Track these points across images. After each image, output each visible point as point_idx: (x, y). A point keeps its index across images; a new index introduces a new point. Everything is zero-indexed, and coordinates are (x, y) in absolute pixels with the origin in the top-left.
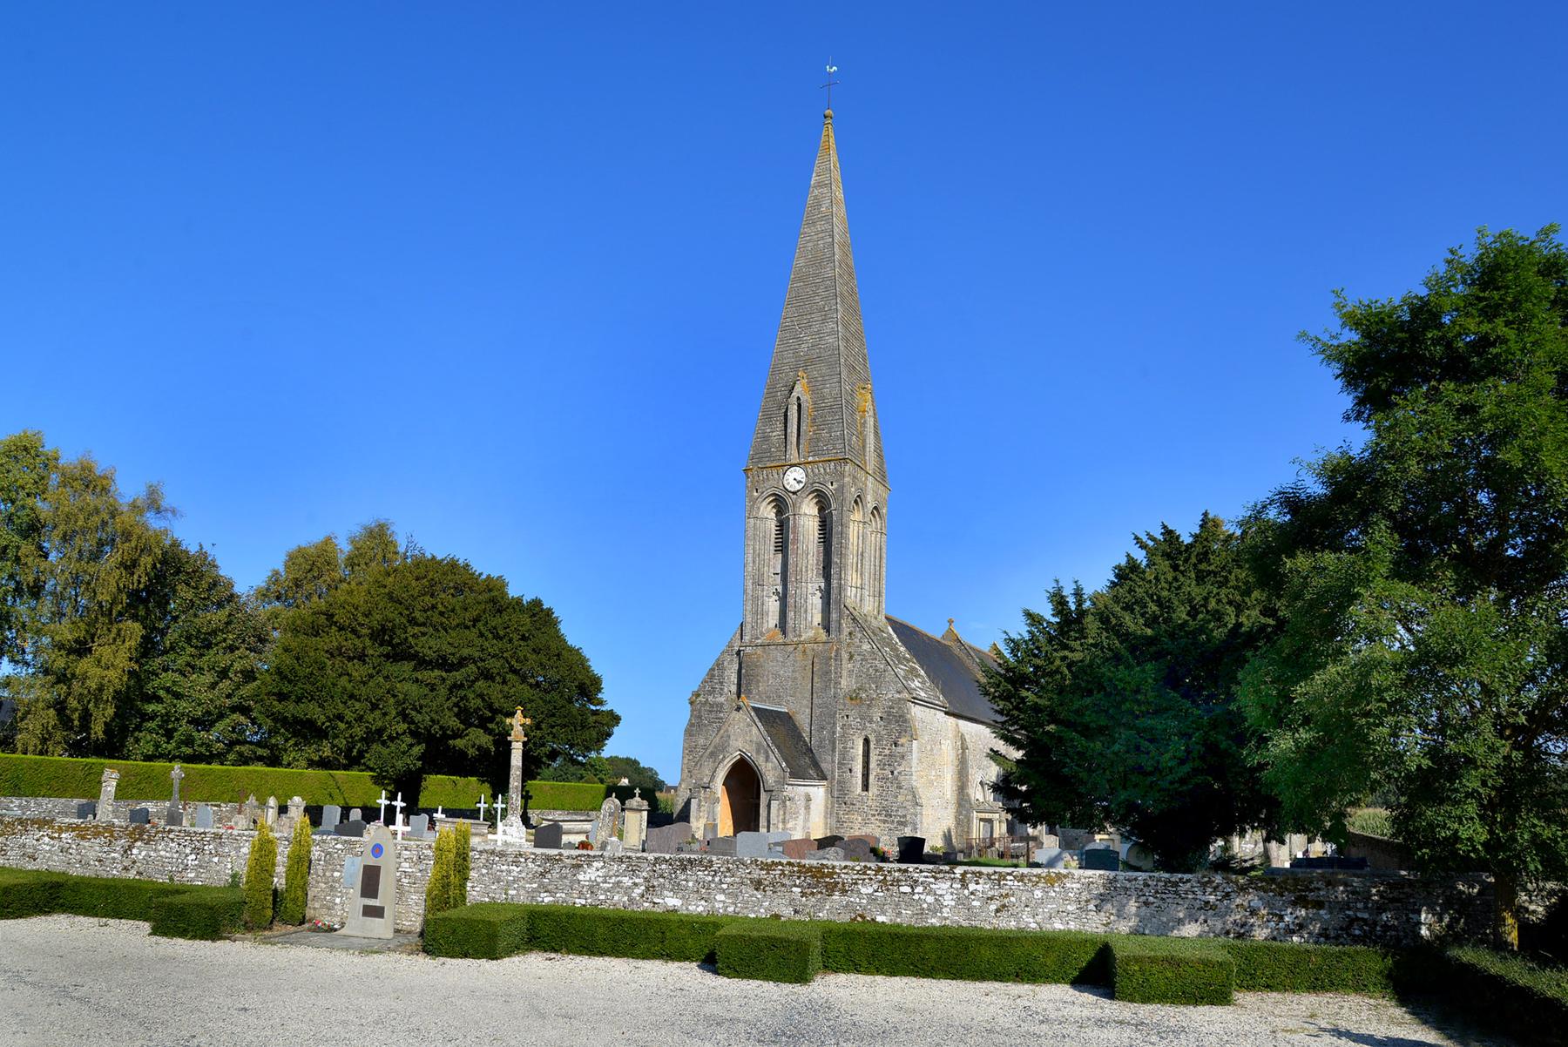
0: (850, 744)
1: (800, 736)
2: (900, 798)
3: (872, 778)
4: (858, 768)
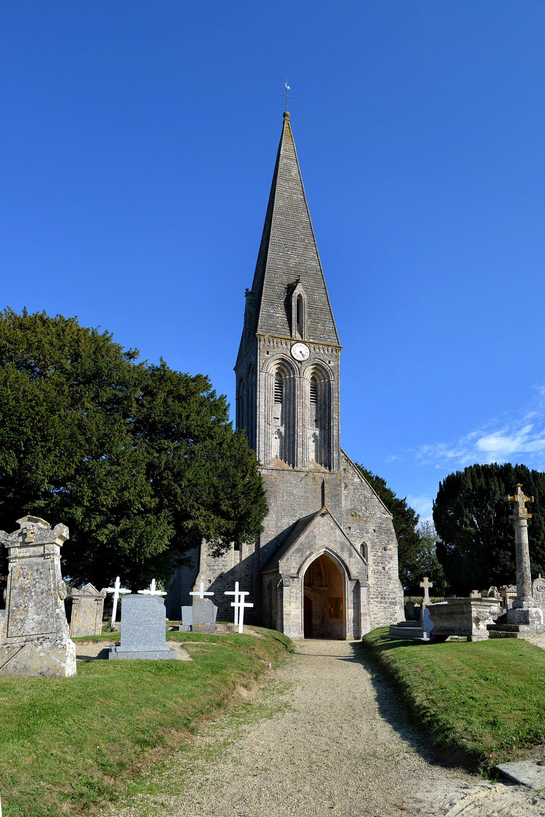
2: (391, 586)
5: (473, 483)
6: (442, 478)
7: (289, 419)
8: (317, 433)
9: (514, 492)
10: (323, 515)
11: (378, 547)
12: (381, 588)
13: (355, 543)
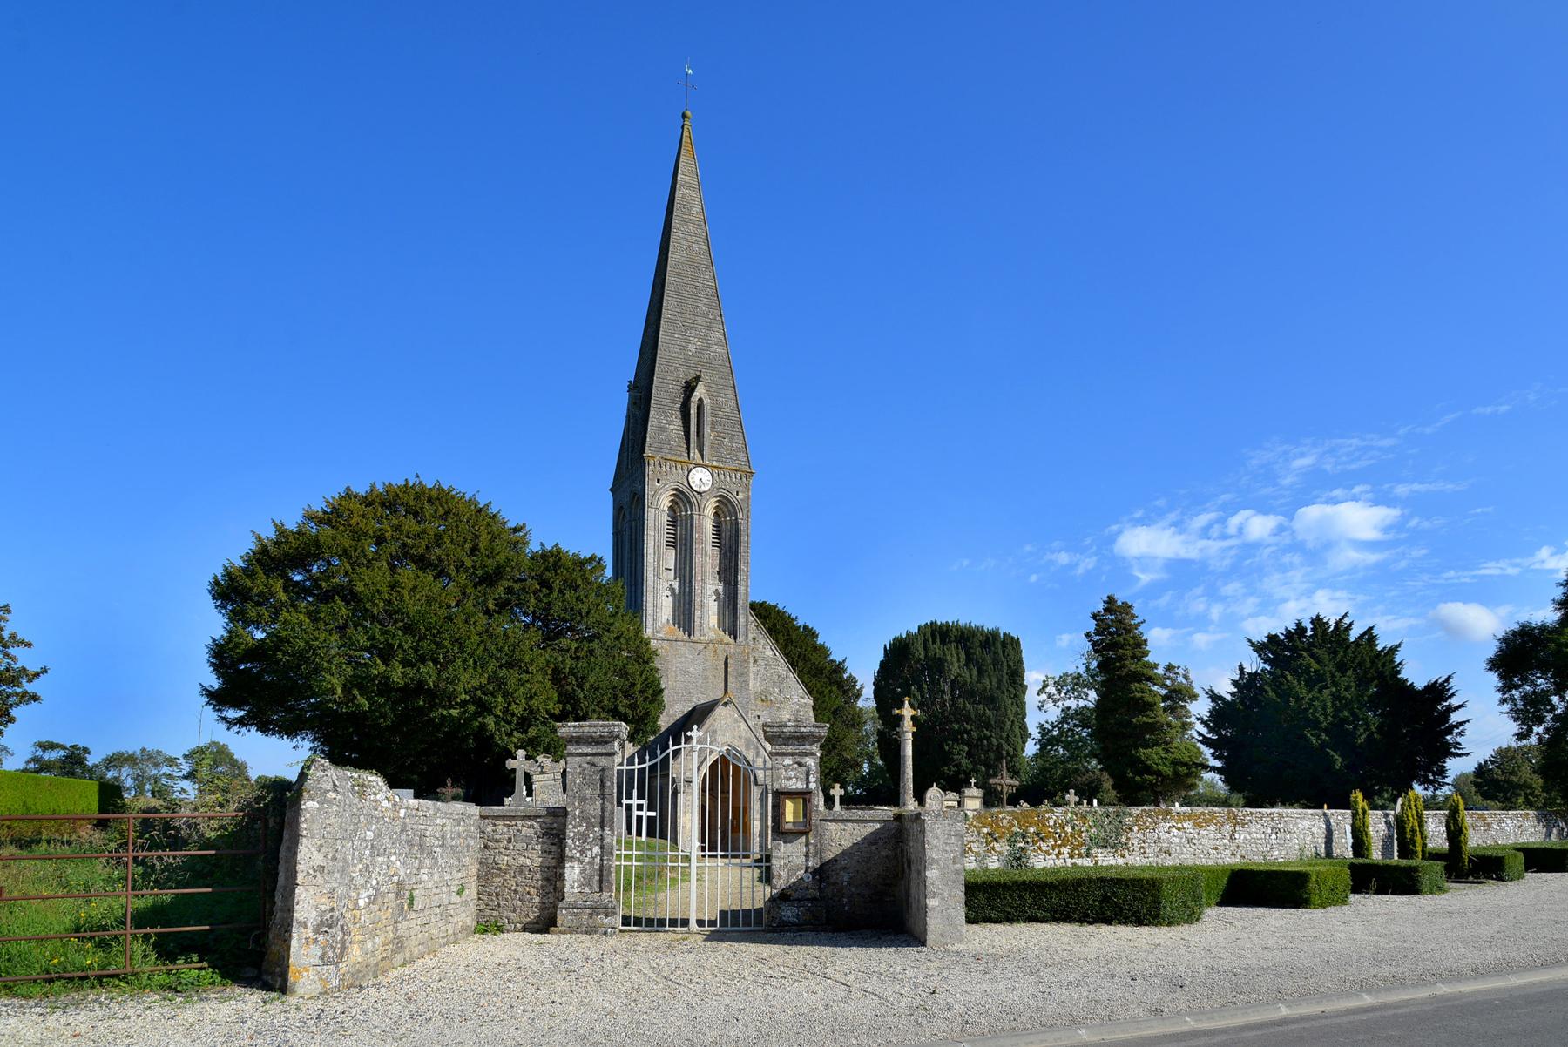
5: (925, 648)
6: (887, 640)
7: (685, 571)
8: (721, 589)
9: (901, 706)
10: (726, 704)
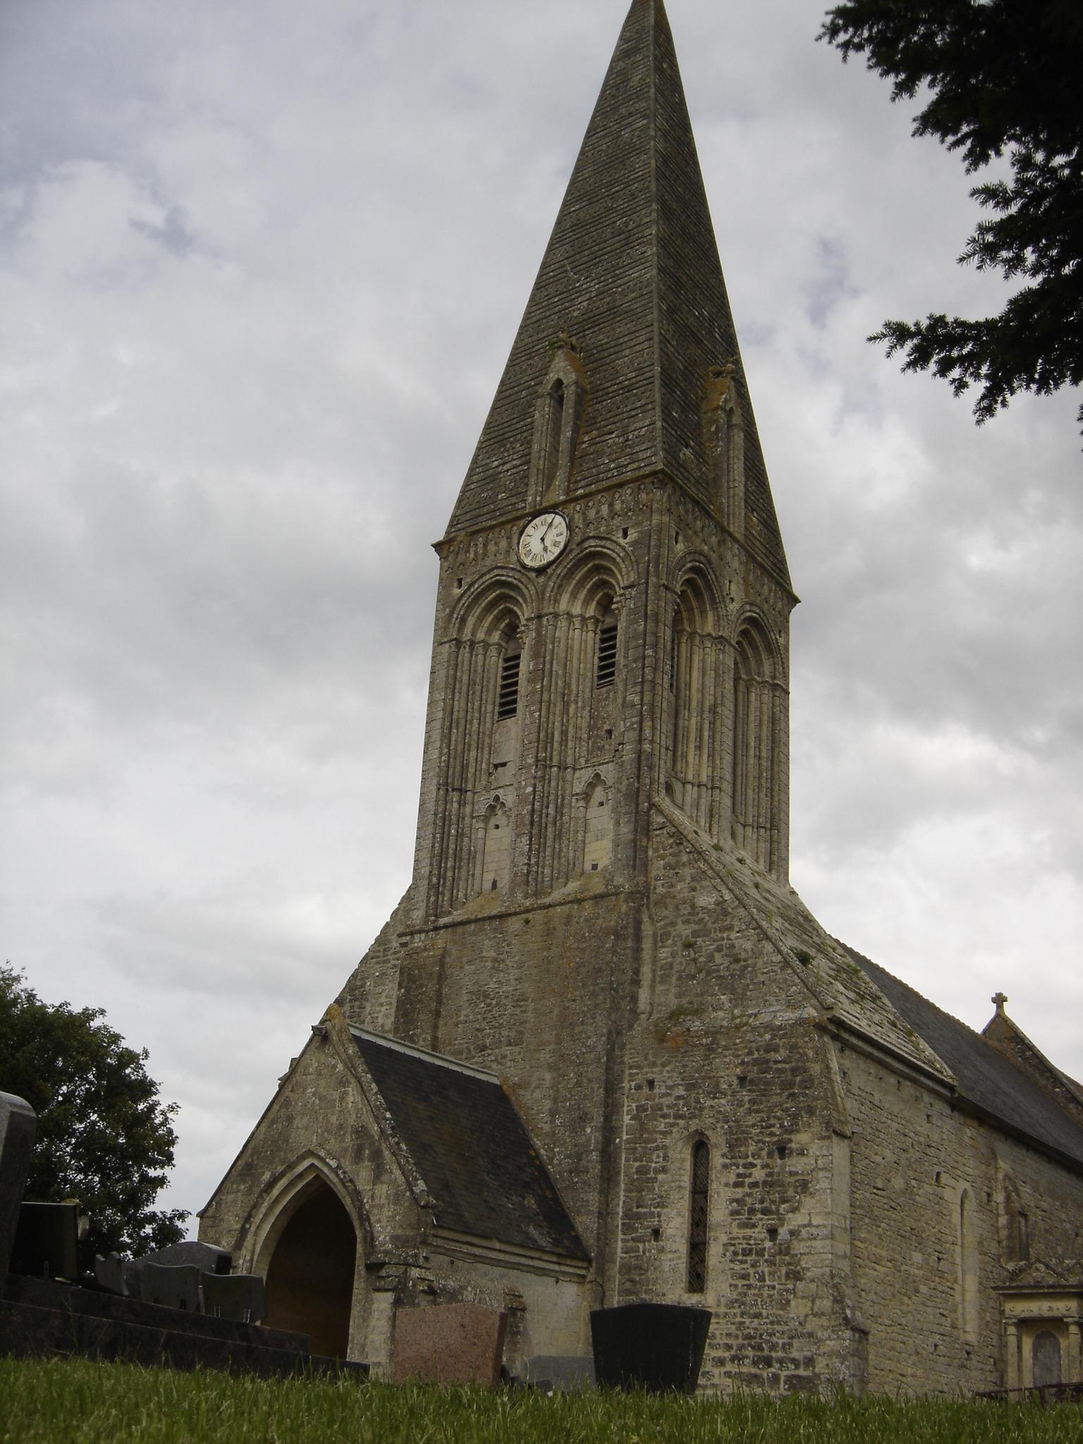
0: (656, 1161)
1: (524, 1145)
2: (798, 1308)
3: (715, 1253)
4: (676, 1225)
11: (752, 1148)
12: (758, 1316)
13: (668, 1141)
